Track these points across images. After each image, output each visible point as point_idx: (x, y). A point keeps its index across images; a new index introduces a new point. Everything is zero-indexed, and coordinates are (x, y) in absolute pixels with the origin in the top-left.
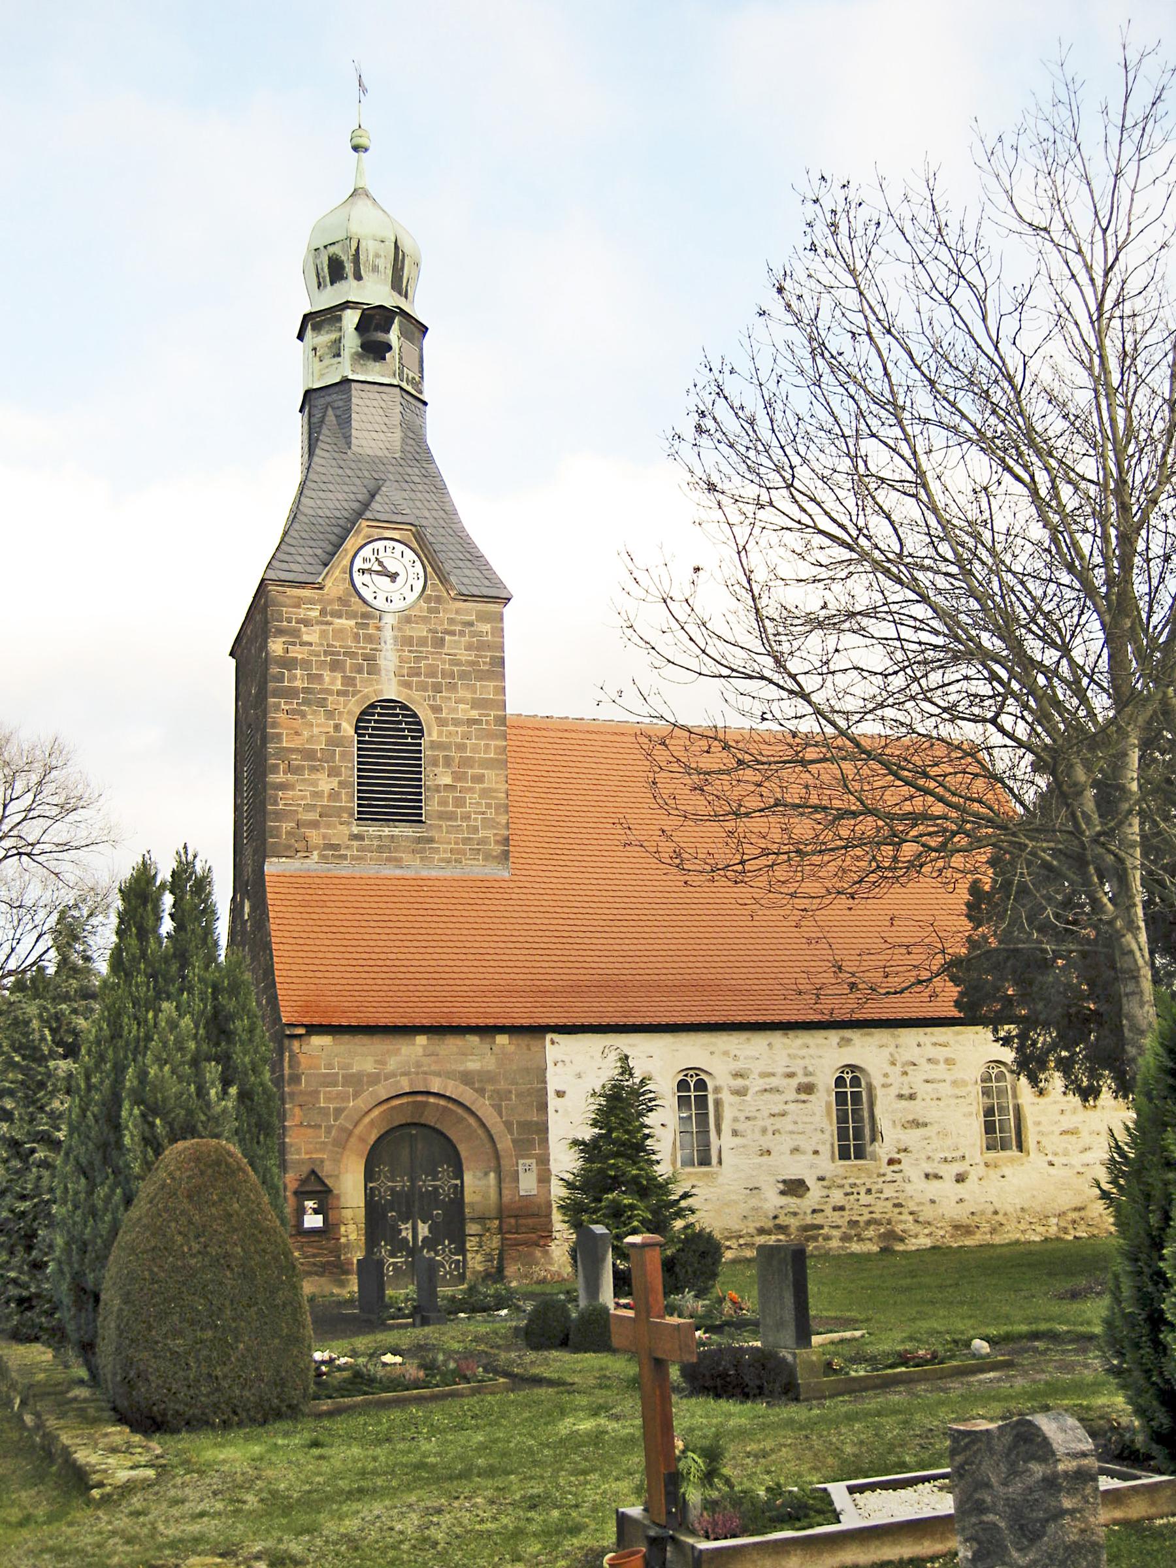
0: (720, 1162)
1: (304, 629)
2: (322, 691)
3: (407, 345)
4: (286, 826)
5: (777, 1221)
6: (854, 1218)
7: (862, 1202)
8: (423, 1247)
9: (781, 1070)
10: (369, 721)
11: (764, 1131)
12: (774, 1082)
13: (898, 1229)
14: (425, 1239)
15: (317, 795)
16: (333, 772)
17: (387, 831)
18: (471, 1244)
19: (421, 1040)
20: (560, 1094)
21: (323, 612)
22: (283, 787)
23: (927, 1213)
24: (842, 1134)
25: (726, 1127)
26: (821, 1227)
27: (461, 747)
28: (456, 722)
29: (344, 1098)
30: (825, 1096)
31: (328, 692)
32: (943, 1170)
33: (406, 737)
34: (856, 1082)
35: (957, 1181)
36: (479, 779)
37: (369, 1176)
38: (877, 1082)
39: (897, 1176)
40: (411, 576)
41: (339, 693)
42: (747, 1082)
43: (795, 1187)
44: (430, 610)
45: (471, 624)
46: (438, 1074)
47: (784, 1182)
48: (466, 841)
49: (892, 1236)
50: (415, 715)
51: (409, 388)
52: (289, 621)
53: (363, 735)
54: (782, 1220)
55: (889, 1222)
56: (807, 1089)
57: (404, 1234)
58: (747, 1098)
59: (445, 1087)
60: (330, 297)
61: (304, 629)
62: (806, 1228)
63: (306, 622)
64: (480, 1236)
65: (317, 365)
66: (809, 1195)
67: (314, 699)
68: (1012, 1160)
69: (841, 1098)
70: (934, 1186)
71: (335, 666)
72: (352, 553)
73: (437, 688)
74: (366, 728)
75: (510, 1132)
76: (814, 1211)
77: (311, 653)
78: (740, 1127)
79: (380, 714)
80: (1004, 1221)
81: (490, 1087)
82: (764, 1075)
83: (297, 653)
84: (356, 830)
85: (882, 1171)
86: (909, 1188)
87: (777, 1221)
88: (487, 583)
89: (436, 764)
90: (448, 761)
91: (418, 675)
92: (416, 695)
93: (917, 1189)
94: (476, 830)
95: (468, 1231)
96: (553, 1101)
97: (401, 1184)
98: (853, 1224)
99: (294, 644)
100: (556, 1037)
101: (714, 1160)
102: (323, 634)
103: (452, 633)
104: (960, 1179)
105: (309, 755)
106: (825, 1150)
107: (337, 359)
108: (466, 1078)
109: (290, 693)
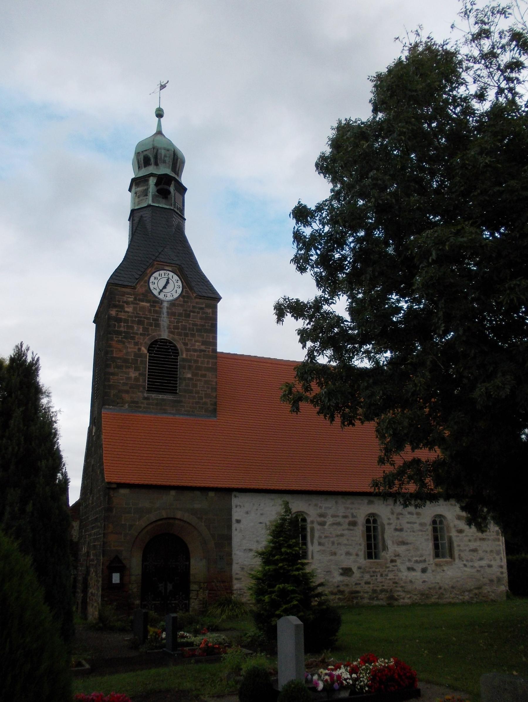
0: (312, 558)
1: (126, 306)
2: (133, 333)
3: (177, 194)
4: (113, 392)
5: (339, 588)
6: (375, 588)
7: (378, 580)
9: (341, 514)
10: (156, 345)
11: (333, 543)
12: (339, 520)
13: (396, 595)
15: (129, 378)
16: (136, 369)
17: (161, 396)
18: (193, 595)
19: (173, 493)
20: (238, 521)
21: (135, 299)
22: (113, 374)
23: (409, 587)
24: (369, 546)
25: (316, 542)
26: (358, 592)
27: (196, 361)
28: (195, 350)
30: (360, 529)
31: (137, 334)
32: (416, 566)
33: (171, 356)
34: (375, 521)
36: (204, 376)
37: (144, 559)
38: (385, 522)
39: (395, 568)
40: (176, 286)
41: (141, 334)
42: (325, 520)
43: (347, 572)
44: (184, 302)
45: (202, 308)
47: (342, 569)
48: (197, 403)
49: (392, 598)
50: (175, 346)
51: (178, 212)
52: (119, 301)
53: (152, 354)
54: (342, 588)
55: (391, 590)
56: (353, 524)
58: (326, 527)
60: (144, 172)
61: (126, 306)
62: (352, 592)
63: (127, 303)
64: (198, 591)
65: (137, 200)
66: (354, 576)
67: (129, 336)
68: (447, 563)
69: (368, 529)
70: (412, 575)
71: (140, 323)
72: (149, 275)
73: (186, 335)
74: (153, 351)
76: (356, 584)
77: (129, 316)
78: (323, 541)
79: (159, 345)
80: (444, 592)
82: (333, 516)
83: (122, 316)
84: (146, 395)
85: (388, 565)
86: (400, 574)
87: (339, 588)
88: (211, 292)
89: (184, 368)
90: (190, 367)
91: (178, 329)
92: (176, 337)
93: (405, 575)
94: (201, 398)
95: (191, 588)
96: (235, 526)
98: (374, 591)
99: (121, 312)
100: (237, 494)
101: (310, 557)
102: (135, 309)
103: (194, 312)
104: (424, 571)
105: (126, 361)
106: (362, 554)
107: (145, 197)
109: (119, 333)
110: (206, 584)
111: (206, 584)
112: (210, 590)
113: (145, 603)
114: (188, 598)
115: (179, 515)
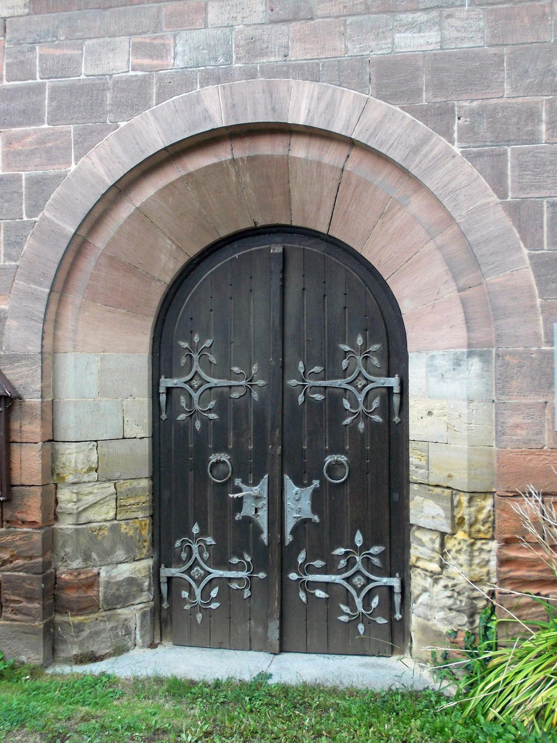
8: (296, 547)
14: (302, 525)
18: (422, 551)
29: (54, 152)
35: (429, 412)
46: (310, 72)
57: (248, 510)
59: (331, 106)
75: (533, 243)
81: (465, 104)
97: (247, 381)
108: (393, 80)
110: (488, 503)
111: (488, 503)
112: (508, 542)
113: (174, 571)
114: (397, 561)
115: (301, 105)
